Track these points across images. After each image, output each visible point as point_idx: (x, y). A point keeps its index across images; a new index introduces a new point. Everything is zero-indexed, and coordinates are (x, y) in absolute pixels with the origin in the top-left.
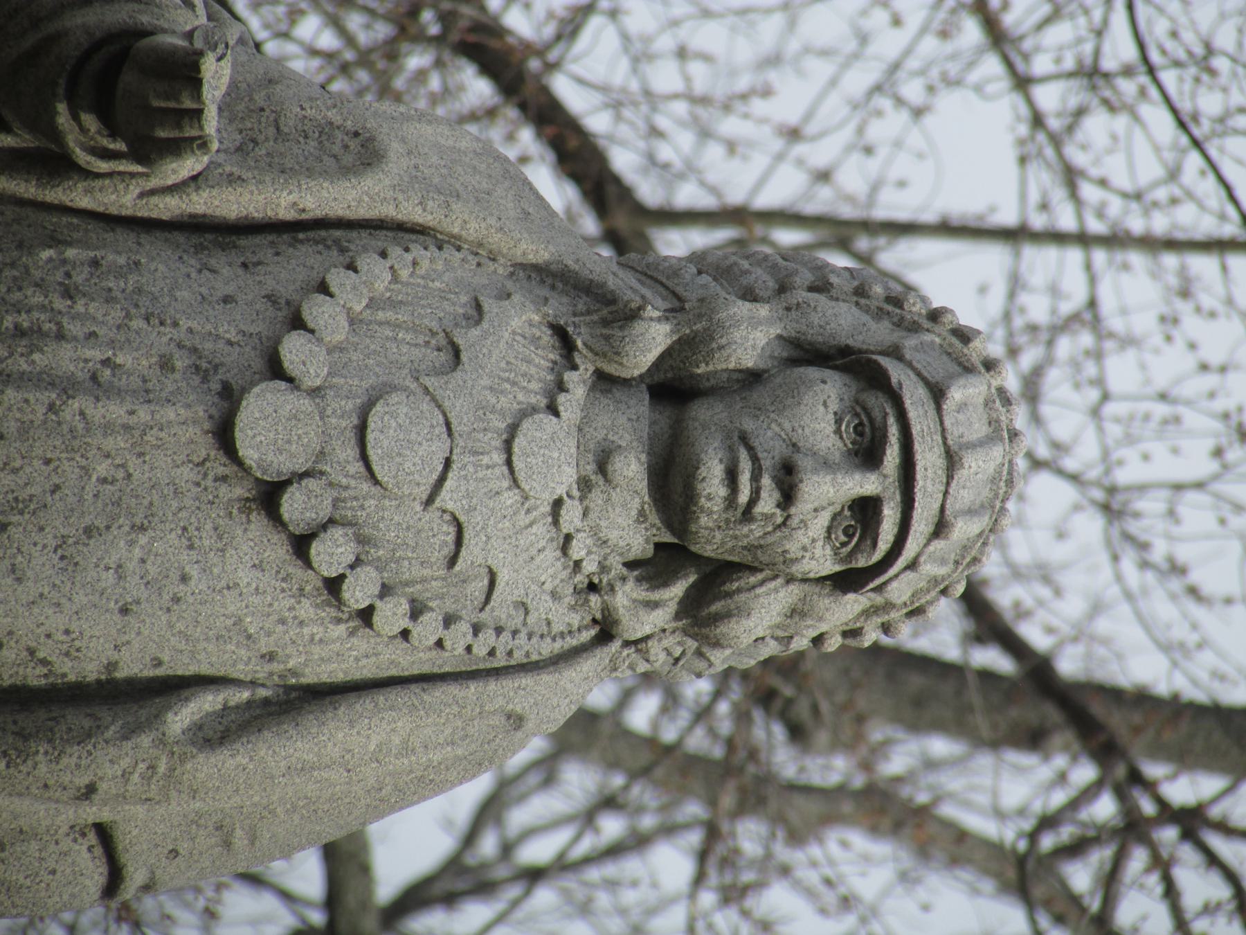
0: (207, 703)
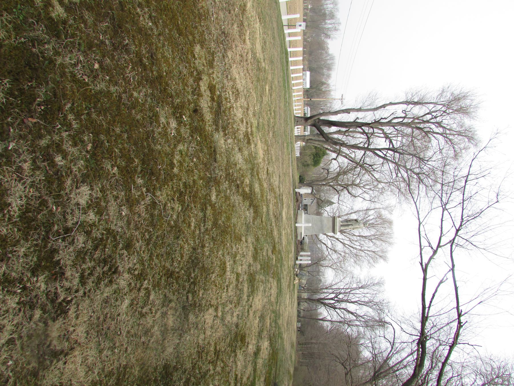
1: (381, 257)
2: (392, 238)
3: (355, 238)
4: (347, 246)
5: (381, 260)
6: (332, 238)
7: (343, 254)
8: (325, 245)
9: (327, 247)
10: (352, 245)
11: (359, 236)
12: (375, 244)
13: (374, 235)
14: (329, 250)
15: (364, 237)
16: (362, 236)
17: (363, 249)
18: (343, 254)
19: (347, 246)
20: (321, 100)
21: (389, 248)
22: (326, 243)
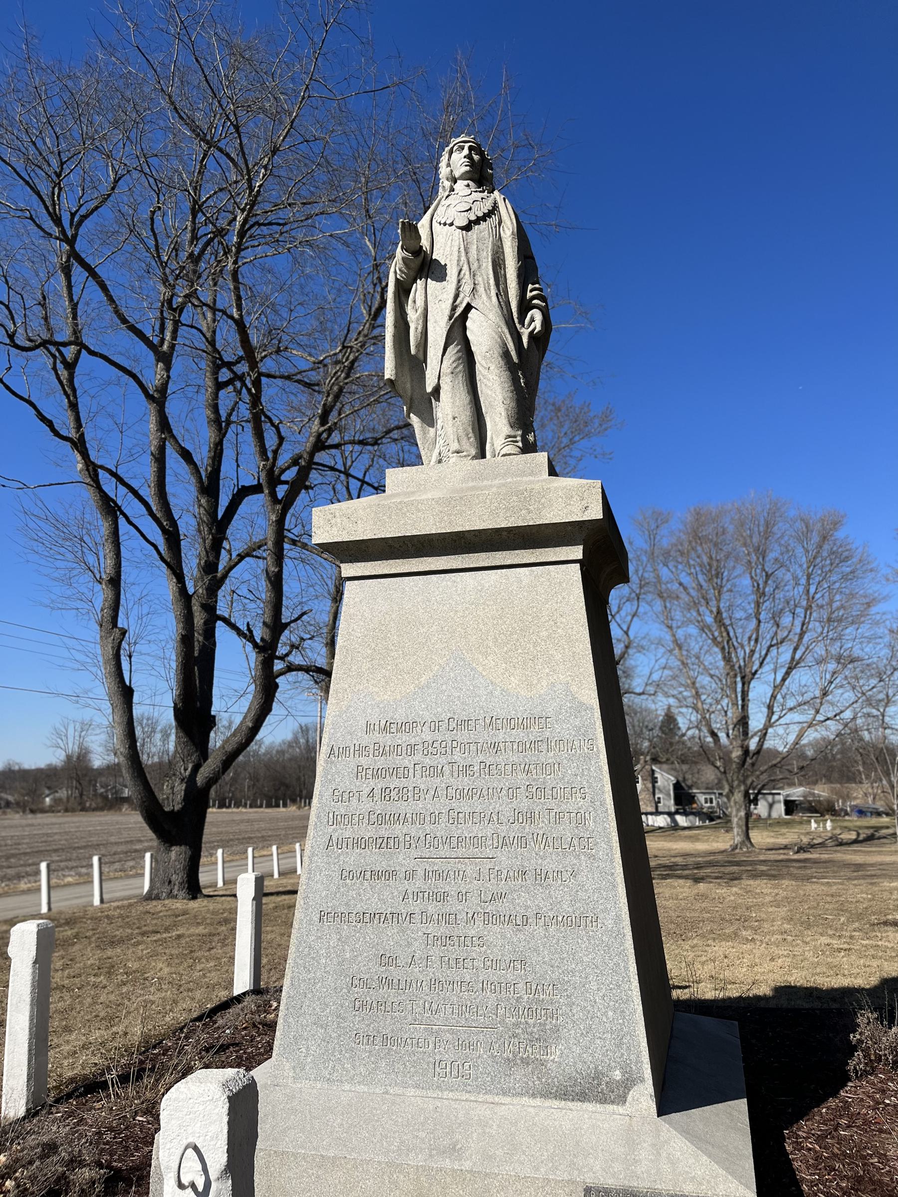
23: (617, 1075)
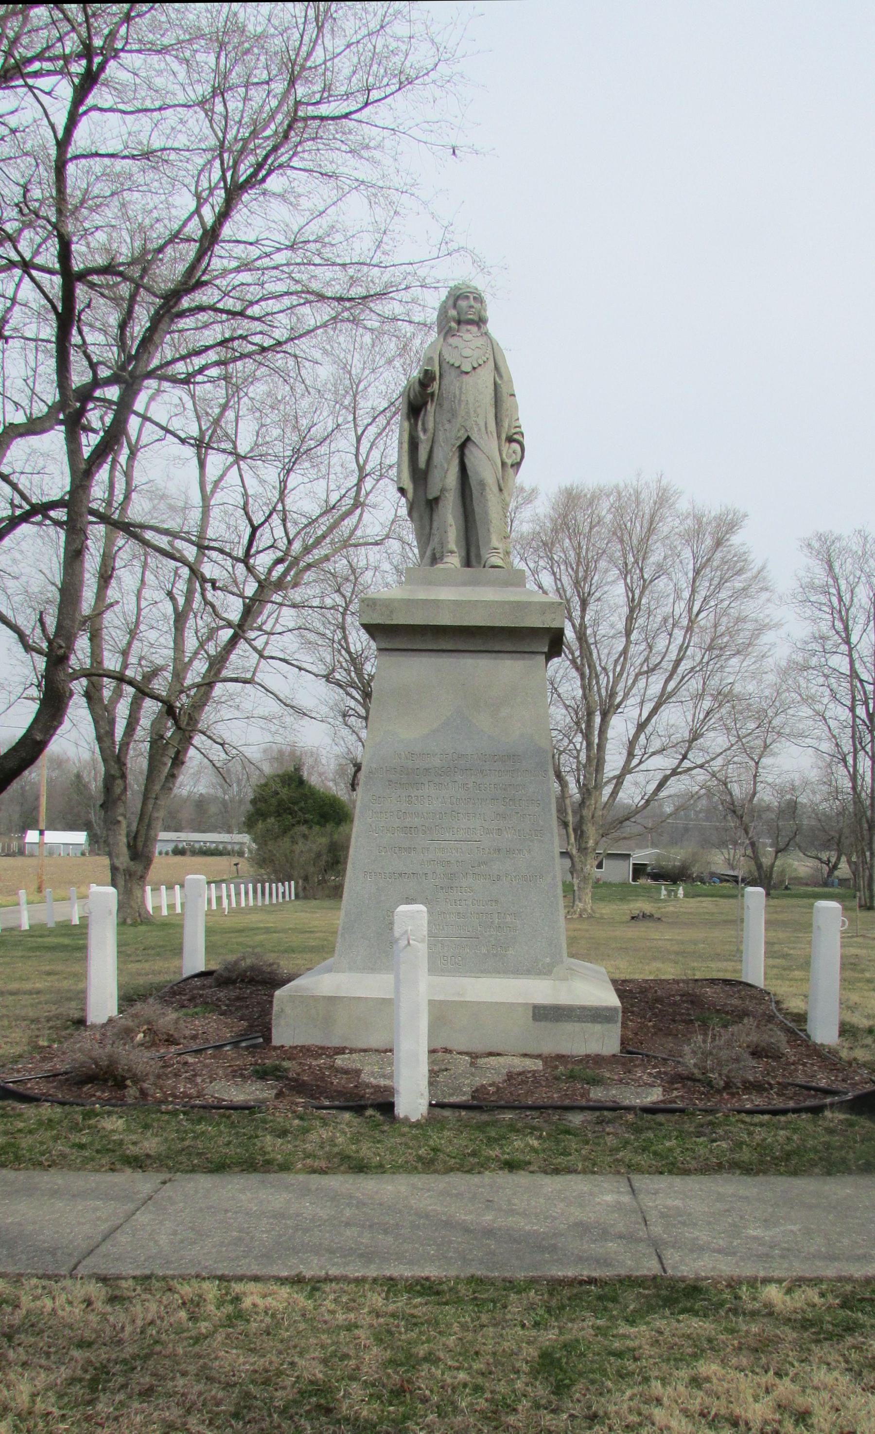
0: (497, 379)
1: (718, 543)
2: (637, 493)
3: (637, 650)
4: (672, 685)
5: (736, 539)
6: (638, 752)
7: (707, 704)
8: (666, 779)
9: (674, 772)
10: (667, 665)
11: (628, 633)
12: (661, 570)
13: (625, 572)
14: (686, 764)
15: (632, 610)
16: (630, 619)
17: (685, 622)
18: (707, 704)
19: (672, 685)
20: (43, 801)
21: (683, 505)
22: (659, 776)
23: (548, 960)
